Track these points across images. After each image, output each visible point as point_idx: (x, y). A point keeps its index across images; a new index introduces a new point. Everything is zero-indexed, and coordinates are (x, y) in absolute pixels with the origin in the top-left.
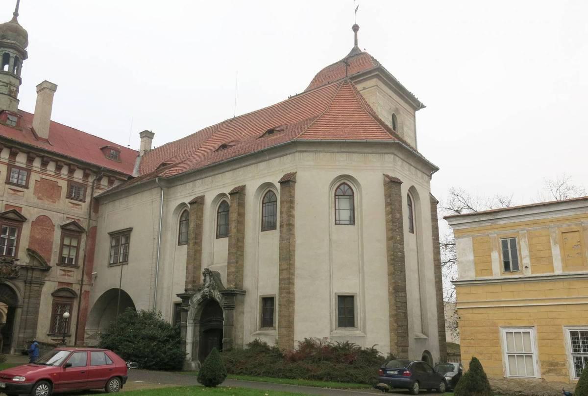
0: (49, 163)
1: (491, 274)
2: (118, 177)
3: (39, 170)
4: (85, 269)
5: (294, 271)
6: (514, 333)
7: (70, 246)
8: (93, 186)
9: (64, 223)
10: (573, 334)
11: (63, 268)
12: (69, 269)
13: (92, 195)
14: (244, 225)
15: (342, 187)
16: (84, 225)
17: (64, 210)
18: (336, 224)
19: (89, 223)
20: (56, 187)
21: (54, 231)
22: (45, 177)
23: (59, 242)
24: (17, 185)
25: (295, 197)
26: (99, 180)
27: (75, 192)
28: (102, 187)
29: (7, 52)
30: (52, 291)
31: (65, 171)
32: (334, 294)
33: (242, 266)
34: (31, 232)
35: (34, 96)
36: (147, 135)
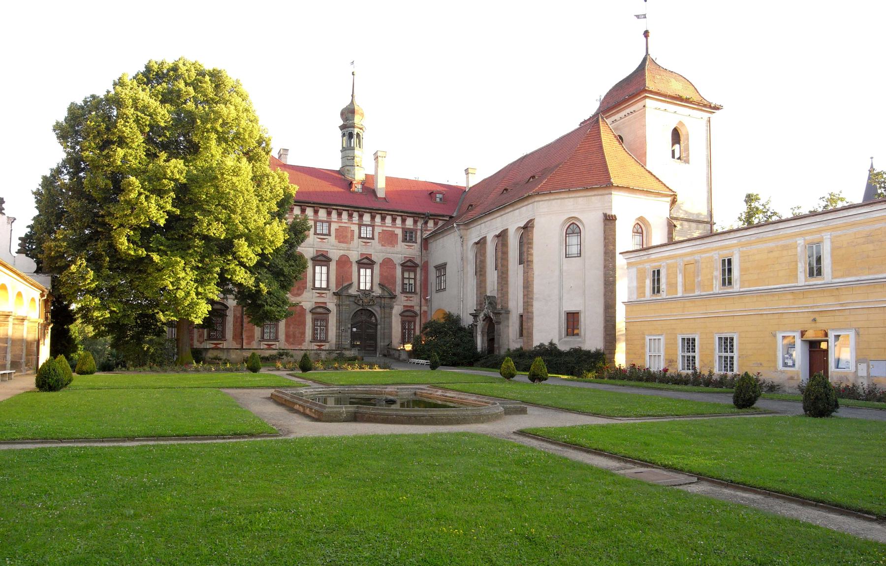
1: (644, 296)
10: (683, 339)
16: (418, 261)
17: (401, 251)
20: (393, 235)
24: (322, 234)
26: (426, 223)
27: (409, 235)
31: (399, 221)
33: (507, 292)
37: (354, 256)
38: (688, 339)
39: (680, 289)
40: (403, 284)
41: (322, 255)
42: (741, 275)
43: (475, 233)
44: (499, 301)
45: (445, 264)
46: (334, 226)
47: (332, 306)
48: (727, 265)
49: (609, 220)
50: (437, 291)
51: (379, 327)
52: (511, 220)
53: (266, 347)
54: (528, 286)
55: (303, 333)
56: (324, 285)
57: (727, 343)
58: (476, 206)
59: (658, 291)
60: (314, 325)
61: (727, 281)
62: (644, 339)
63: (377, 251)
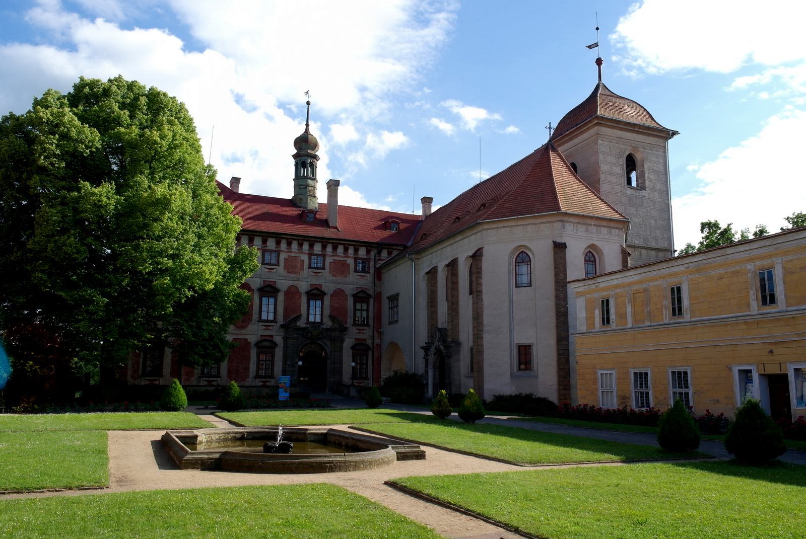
0: (338, 246)
2: (395, 248)
3: (331, 254)
4: (375, 326)
5: (483, 328)
6: (609, 375)
7: (361, 310)
8: (375, 259)
9: (355, 292)
10: (635, 374)
11: (358, 328)
12: (362, 328)
13: (375, 266)
14: (458, 291)
15: (521, 255)
16: (371, 292)
17: (353, 282)
18: (516, 287)
19: (374, 290)
20: (345, 265)
21: (347, 299)
22: (336, 258)
23: (352, 308)
24: (317, 268)
25: (483, 268)
26: (379, 253)
28: (382, 258)
29: (303, 160)
30: (351, 346)
32: (515, 345)
33: (458, 324)
34: (330, 302)
35: (326, 191)
36: (427, 201)
37: (304, 286)
38: (641, 374)
39: (630, 319)
40: (355, 316)
41: (269, 286)
42: (691, 304)
43: (428, 260)
44: (449, 333)
45: (398, 295)
46: (283, 256)
47: (279, 339)
48: (676, 293)
49: (560, 248)
50: (390, 323)
51: (329, 361)
52: (461, 249)
53: (206, 383)
54: (478, 317)
55: (247, 369)
56: (271, 317)
57: (681, 378)
58: (430, 235)
59: (608, 322)
60: (259, 360)
61: (677, 310)
62: (596, 373)
63: (327, 281)
